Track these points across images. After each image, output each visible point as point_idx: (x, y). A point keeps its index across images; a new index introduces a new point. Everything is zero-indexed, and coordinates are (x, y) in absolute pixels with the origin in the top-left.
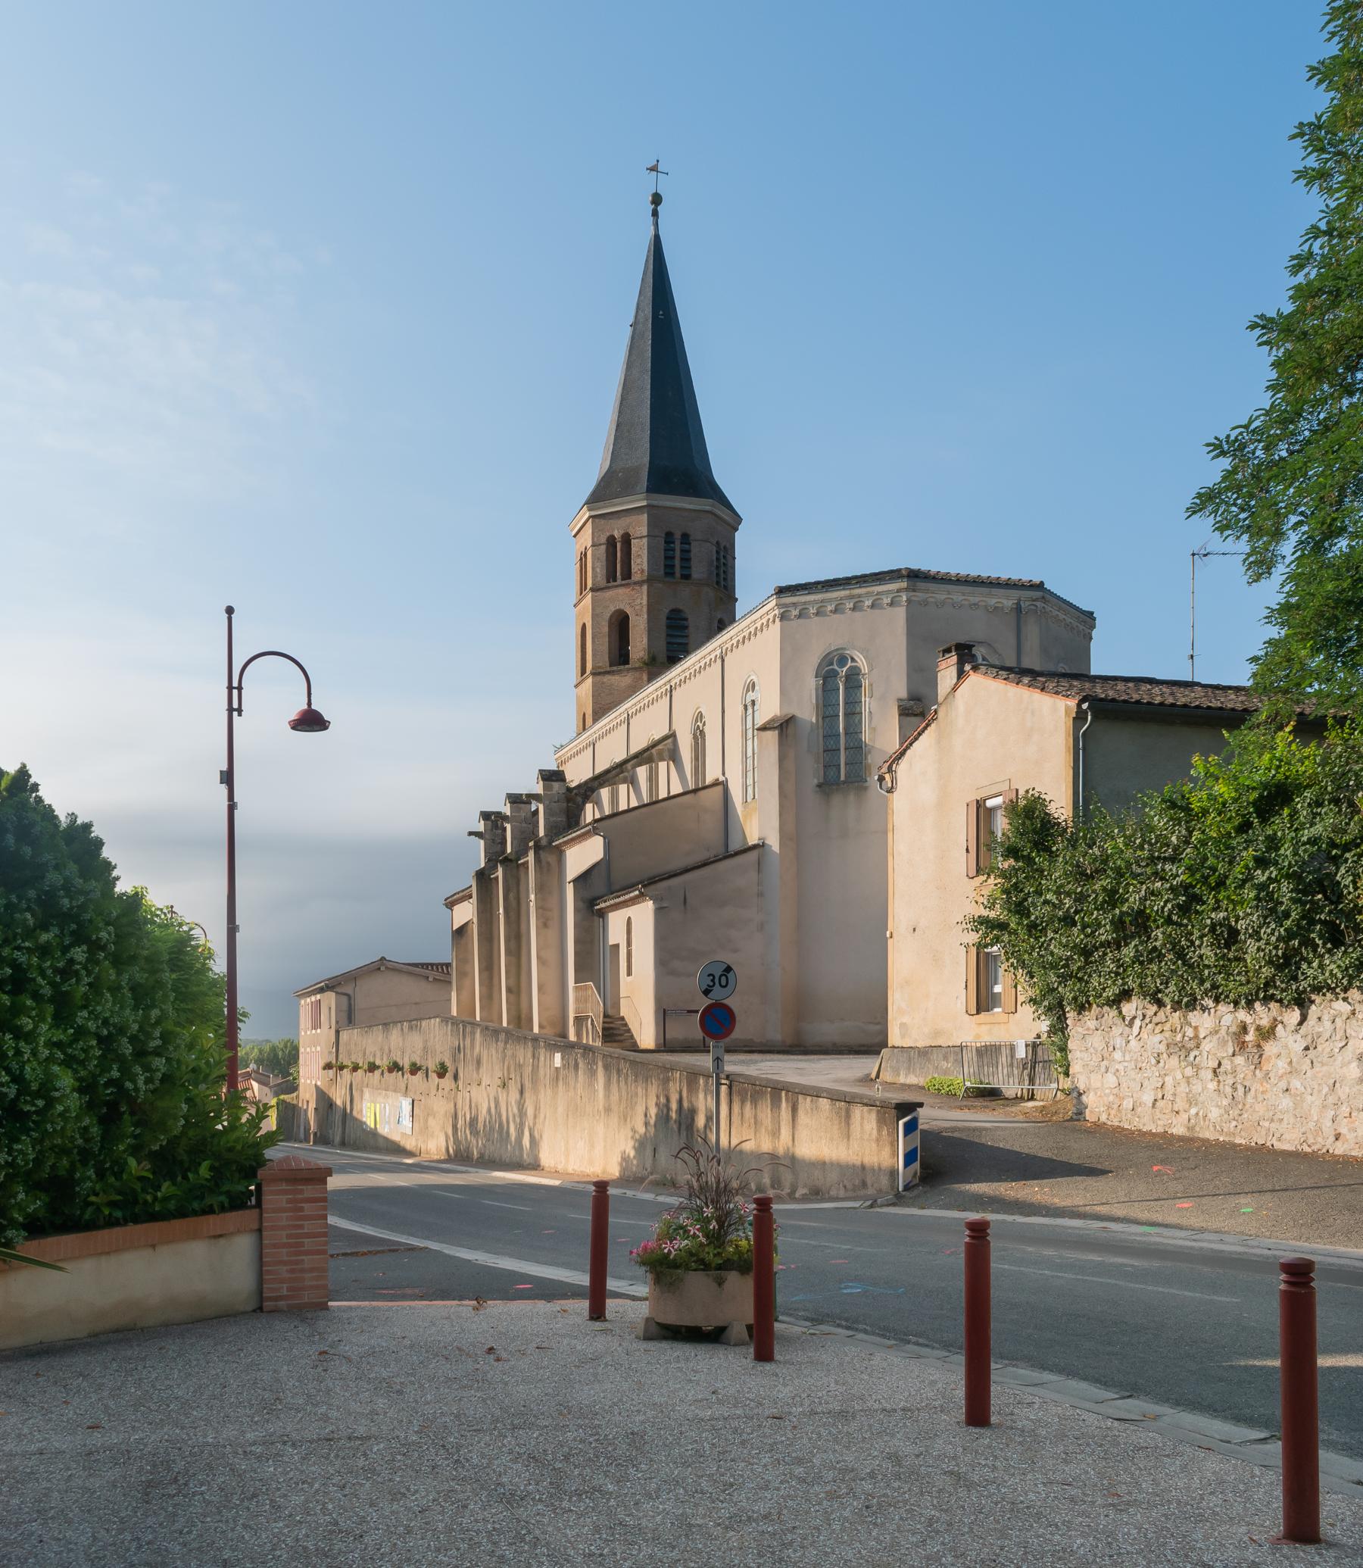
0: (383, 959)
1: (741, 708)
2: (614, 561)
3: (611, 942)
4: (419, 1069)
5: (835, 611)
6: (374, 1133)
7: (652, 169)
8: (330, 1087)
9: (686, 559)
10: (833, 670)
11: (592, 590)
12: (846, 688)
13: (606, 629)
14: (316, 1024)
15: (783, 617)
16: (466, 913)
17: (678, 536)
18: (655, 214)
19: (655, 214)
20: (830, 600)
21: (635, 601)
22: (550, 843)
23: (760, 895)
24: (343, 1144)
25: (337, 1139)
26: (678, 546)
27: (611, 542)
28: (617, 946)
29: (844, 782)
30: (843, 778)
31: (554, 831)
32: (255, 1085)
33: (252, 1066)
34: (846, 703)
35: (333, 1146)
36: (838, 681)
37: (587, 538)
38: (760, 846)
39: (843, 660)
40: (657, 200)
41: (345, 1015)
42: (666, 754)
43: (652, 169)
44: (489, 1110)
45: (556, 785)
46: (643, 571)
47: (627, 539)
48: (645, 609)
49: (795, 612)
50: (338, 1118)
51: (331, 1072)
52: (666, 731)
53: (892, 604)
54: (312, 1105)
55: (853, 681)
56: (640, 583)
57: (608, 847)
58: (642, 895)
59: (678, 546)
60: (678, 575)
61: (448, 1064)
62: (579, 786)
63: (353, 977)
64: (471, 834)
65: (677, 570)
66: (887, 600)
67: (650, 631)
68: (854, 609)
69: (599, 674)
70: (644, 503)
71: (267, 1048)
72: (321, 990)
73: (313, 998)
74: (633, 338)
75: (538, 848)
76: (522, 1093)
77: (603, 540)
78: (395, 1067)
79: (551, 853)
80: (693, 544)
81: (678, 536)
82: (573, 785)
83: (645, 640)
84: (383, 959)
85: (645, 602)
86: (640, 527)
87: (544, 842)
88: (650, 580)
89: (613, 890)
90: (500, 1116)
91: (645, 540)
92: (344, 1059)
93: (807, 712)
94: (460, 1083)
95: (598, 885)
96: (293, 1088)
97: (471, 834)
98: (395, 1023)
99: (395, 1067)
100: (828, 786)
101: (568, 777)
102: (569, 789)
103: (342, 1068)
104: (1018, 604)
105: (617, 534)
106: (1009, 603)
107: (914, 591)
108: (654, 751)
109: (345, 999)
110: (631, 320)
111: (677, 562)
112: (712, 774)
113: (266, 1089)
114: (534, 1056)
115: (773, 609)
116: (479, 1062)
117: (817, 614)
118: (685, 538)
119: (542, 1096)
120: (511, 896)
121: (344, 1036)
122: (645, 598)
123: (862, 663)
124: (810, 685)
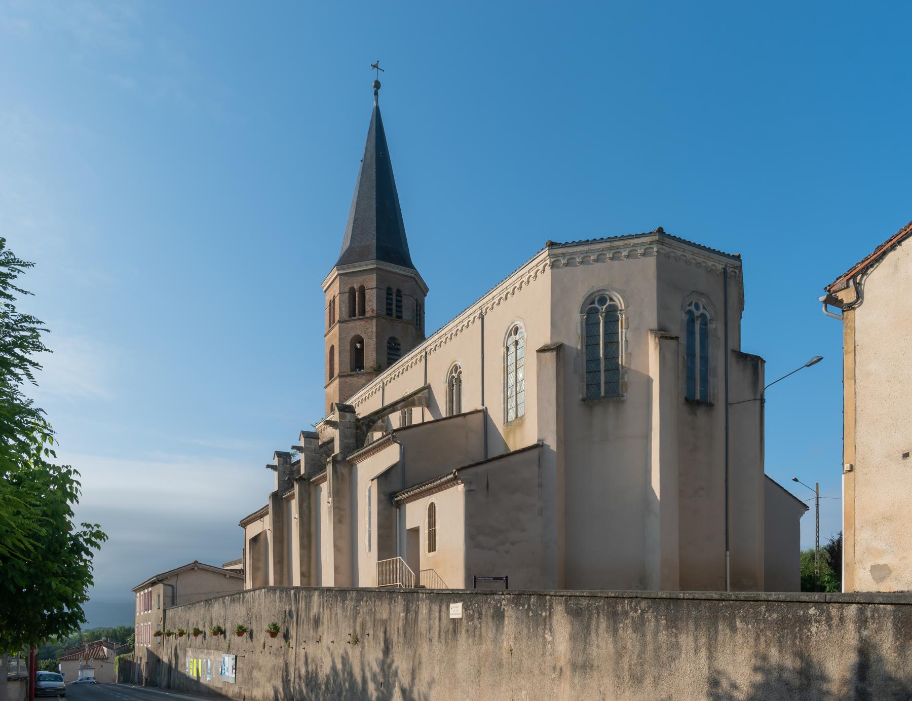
0: (196, 562)
1: (503, 350)
2: (355, 304)
3: (409, 526)
4: (245, 631)
5: (597, 261)
6: (197, 682)
7: (375, 66)
8: (158, 648)
9: (399, 307)
10: (595, 308)
11: (339, 322)
12: (605, 323)
13: (348, 348)
14: (148, 607)
15: (553, 266)
16: (265, 525)
17: (394, 290)
18: (376, 94)
19: (376, 94)
20: (593, 251)
21: (368, 331)
22: (344, 459)
23: (540, 486)
24: (169, 687)
25: (164, 683)
26: (394, 297)
27: (352, 291)
28: (416, 531)
29: (604, 397)
30: (603, 394)
31: (347, 449)
32: (105, 649)
33: (103, 638)
34: (605, 334)
35: (160, 688)
36: (599, 316)
37: (335, 290)
38: (539, 446)
39: (602, 301)
40: (377, 85)
41: (169, 600)
42: (423, 401)
43: (375, 66)
44: (334, 668)
45: (348, 415)
46: (373, 310)
47: (362, 290)
48: (374, 335)
49: (563, 261)
50: (164, 670)
51: (159, 639)
52: (422, 385)
53: (644, 255)
54: (144, 661)
55: (612, 316)
56: (371, 318)
57: (403, 453)
58: (456, 478)
59: (394, 297)
60: (394, 315)
61: (280, 624)
62: (364, 418)
63: (176, 573)
64: (268, 466)
65: (394, 312)
66: (640, 251)
67: (378, 348)
68: (612, 259)
69: (344, 376)
70: (374, 266)
71: (111, 631)
72: (153, 584)
73: (146, 591)
74: (363, 168)
75: (335, 461)
76: (387, 651)
77: (347, 290)
78: (219, 631)
79: (345, 468)
80: (404, 297)
81: (394, 290)
82: (360, 417)
83: (374, 355)
84: (196, 562)
85: (374, 330)
86: (371, 282)
87: (339, 458)
88: (378, 316)
89: (405, 487)
90: (351, 674)
91: (375, 291)
92: (169, 627)
93: (574, 341)
94: (293, 642)
95: (396, 485)
96: (130, 649)
97: (268, 466)
98: (217, 598)
99: (219, 631)
100: (591, 399)
101: (357, 410)
102: (358, 420)
103: (169, 634)
104: (724, 269)
105: (356, 286)
106: (720, 267)
107: (662, 244)
108: (415, 397)
109: (170, 588)
110: (362, 157)
111: (394, 307)
112: (469, 403)
113: (112, 651)
114: (407, 610)
115: (544, 260)
116: (317, 622)
117: (582, 263)
118: (399, 291)
119: (424, 650)
120: (305, 505)
121: (170, 613)
122: (374, 328)
123: (620, 302)
124: (576, 318)
